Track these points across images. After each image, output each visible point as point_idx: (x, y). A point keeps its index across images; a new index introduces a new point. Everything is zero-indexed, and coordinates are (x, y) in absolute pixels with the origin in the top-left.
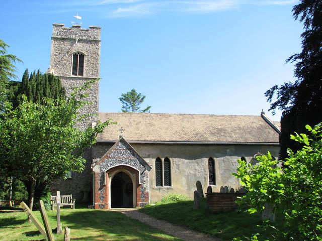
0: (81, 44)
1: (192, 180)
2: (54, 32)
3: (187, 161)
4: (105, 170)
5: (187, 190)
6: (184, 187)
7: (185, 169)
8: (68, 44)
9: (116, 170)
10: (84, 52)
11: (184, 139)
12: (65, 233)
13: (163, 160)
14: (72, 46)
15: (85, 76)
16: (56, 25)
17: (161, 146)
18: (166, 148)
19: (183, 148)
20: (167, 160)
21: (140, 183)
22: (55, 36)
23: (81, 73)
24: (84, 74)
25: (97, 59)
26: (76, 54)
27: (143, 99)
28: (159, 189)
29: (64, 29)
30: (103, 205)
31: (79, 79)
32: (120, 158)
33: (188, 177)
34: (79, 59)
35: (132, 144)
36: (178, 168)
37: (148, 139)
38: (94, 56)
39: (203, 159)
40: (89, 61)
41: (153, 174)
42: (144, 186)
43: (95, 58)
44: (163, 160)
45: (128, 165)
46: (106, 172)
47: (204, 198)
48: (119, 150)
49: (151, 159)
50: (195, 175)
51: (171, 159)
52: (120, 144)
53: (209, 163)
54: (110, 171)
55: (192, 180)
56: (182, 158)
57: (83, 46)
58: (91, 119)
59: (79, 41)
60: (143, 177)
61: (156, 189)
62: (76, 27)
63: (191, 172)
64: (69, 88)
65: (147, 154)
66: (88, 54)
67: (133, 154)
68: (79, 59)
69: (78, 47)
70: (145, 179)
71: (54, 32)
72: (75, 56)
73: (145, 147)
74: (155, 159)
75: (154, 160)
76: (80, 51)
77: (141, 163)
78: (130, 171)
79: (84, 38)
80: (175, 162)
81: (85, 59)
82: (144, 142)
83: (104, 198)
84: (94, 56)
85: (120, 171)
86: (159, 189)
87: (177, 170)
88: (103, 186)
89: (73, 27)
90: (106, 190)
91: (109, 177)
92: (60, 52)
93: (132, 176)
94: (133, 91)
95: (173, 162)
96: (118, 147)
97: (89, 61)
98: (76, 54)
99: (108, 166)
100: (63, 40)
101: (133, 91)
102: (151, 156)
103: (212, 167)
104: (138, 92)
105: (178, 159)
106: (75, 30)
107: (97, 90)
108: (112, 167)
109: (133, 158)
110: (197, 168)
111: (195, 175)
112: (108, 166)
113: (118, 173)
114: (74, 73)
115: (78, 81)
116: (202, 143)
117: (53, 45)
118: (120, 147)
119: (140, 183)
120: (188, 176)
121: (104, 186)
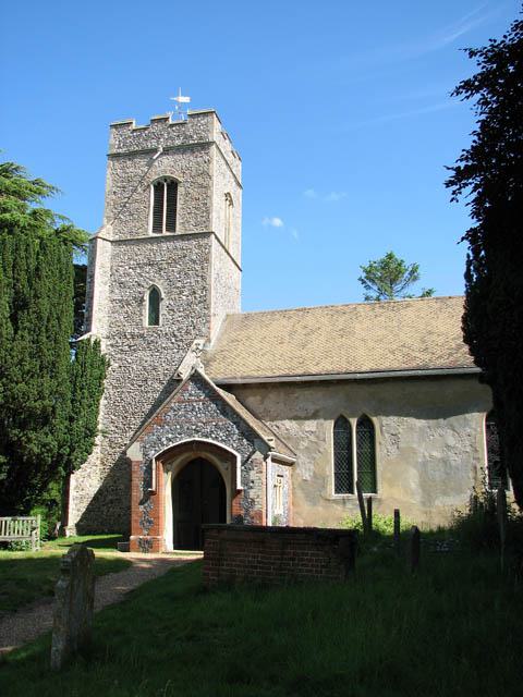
0: (170, 157)
1: (437, 474)
2: (112, 141)
3: (420, 423)
4: (153, 454)
5: (423, 503)
6: (413, 494)
7: (415, 446)
8: (142, 162)
9: (180, 453)
10: (177, 176)
11: (414, 364)
12: (204, 590)
13: (354, 422)
14: (150, 165)
15: (179, 230)
16: (115, 126)
17: (347, 387)
18: (365, 390)
19: (410, 388)
20: (366, 426)
21: (239, 487)
22: (115, 151)
23: (171, 226)
24: (178, 227)
25: (207, 187)
26: (159, 183)
27: (412, 272)
28: (344, 501)
29: (134, 131)
30: (147, 541)
31: (167, 239)
32: (189, 421)
33: (424, 466)
34: (167, 189)
35: (228, 387)
36: (396, 443)
37: (314, 370)
38: (200, 180)
39: (467, 415)
40: (187, 194)
41: (329, 461)
42: (252, 493)
43: (201, 186)
44: (354, 422)
45: (210, 440)
46: (157, 459)
47: (205, 558)
48: (189, 401)
49: (322, 421)
50: (445, 461)
51: (375, 419)
52: (190, 386)
53: (488, 427)
54: (166, 457)
55: (437, 474)
56: (407, 415)
57: (175, 162)
58: (193, 332)
59: (166, 151)
60: (247, 470)
61: (335, 501)
62: (159, 120)
63: (435, 454)
64: (146, 265)
65: (312, 408)
66: (187, 177)
67: (224, 413)
68: (167, 189)
69: (165, 166)
70: (253, 475)
71: (113, 142)
72: (158, 187)
73: (307, 393)
74: (332, 423)
75: (330, 425)
76: (168, 174)
77: (242, 434)
78: (211, 452)
79: (178, 142)
80: (385, 425)
81: (181, 190)
82: (423, 373)
83: (153, 524)
84: (200, 180)
85: (193, 457)
86: (344, 501)
87: (393, 449)
88: (150, 495)
89: (153, 121)
90: (157, 503)
91: (167, 471)
92: (125, 184)
93: (222, 467)
94: (390, 256)
95: (382, 426)
96: (186, 395)
97: (187, 194)
98: (159, 183)
99: (163, 445)
100: (131, 155)
101: (390, 256)
102: (321, 413)
103: (345, 452)
104: (398, 256)
105: (396, 418)
106: (157, 128)
107: (207, 260)
108: (171, 445)
109: (224, 421)
110: (451, 441)
111: (445, 461)
112: (163, 445)
113: (192, 462)
114: (157, 227)
115: (164, 246)
116: (461, 371)
117: (109, 171)
118: (190, 395)
119: (239, 487)
120: (424, 464)
121: (153, 493)
